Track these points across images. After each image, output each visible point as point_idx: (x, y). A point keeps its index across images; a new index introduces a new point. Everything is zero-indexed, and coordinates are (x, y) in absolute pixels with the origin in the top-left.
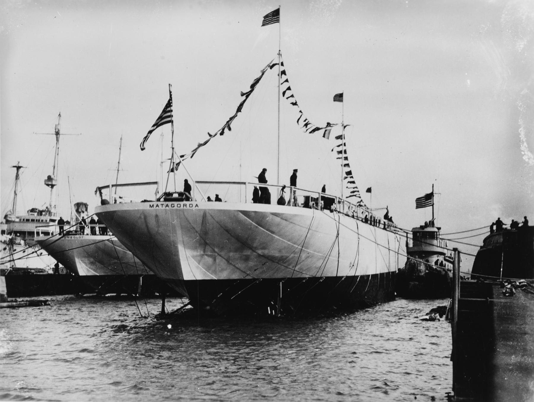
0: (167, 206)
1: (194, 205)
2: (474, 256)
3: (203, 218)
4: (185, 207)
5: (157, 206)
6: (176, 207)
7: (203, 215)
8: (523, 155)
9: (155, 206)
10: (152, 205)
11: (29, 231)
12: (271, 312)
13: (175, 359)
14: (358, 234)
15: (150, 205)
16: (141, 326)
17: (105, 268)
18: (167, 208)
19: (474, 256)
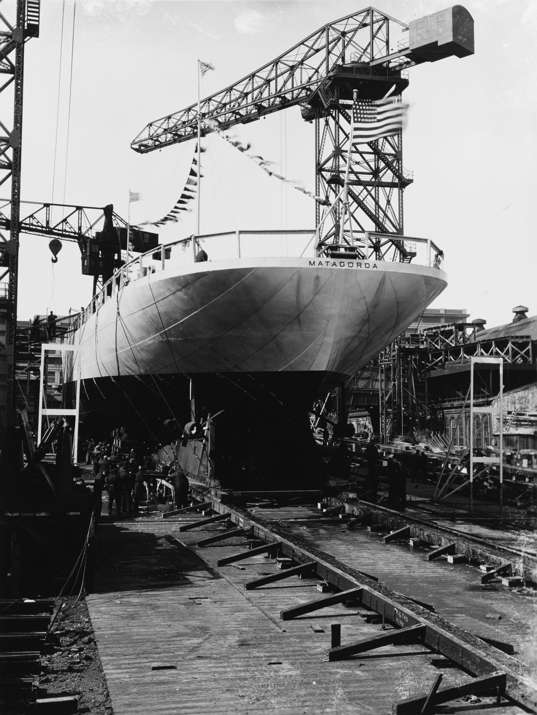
0: (334, 264)
1: (372, 265)
2: (357, 208)
3: (380, 283)
4: (359, 266)
5: (320, 263)
6: (346, 267)
7: (381, 280)
8: (388, 66)
9: (317, 263)
10: (312, 263)
11: (95, 377)
12: (141, 509)
13: (398, 598)
14: (160, 127)
15: (310, 262)
16: (440, 493)
17: (160, 451)
18: (334, 267)
19: (357, 208)
